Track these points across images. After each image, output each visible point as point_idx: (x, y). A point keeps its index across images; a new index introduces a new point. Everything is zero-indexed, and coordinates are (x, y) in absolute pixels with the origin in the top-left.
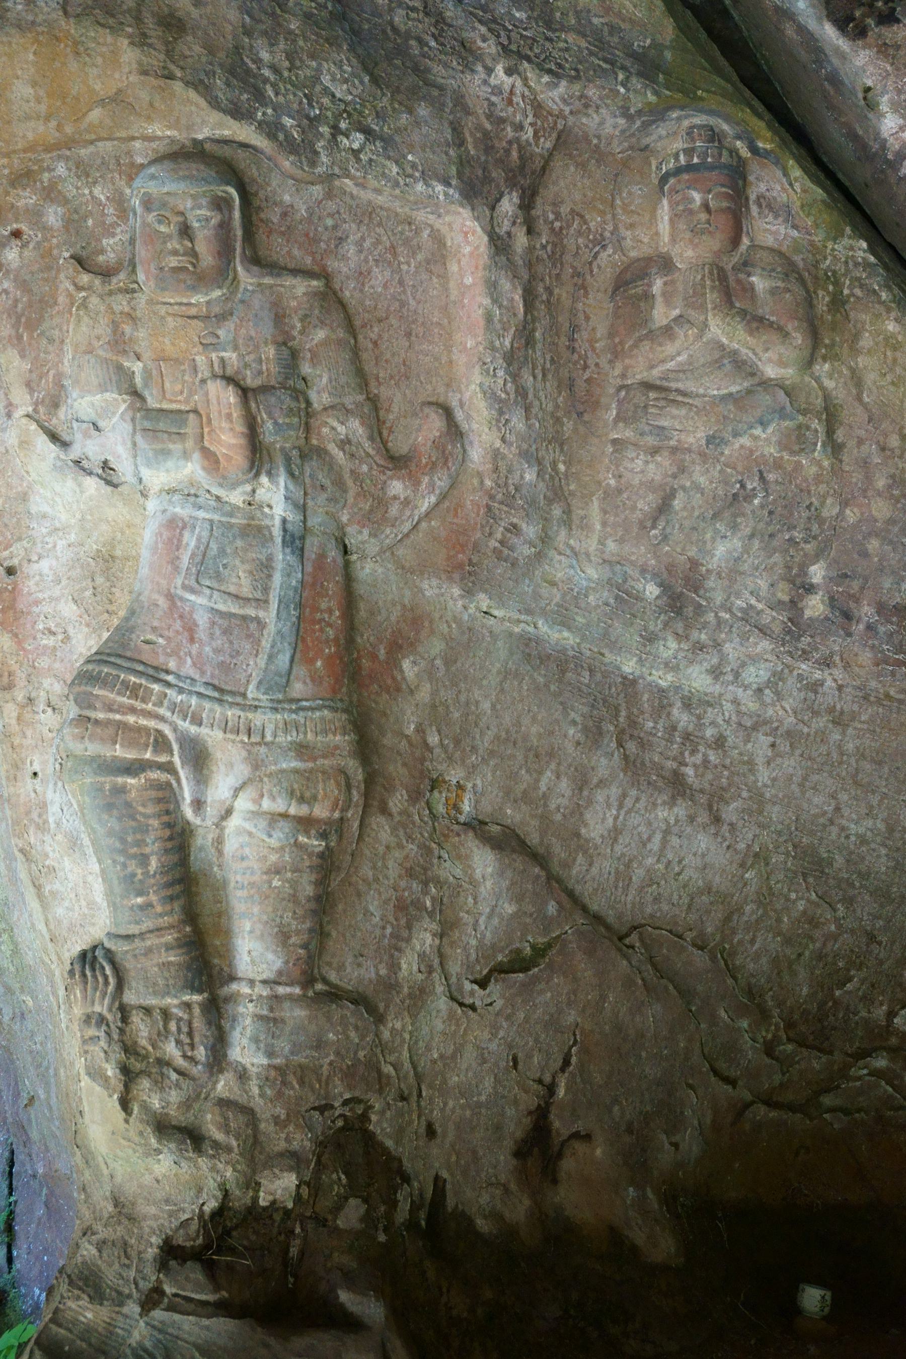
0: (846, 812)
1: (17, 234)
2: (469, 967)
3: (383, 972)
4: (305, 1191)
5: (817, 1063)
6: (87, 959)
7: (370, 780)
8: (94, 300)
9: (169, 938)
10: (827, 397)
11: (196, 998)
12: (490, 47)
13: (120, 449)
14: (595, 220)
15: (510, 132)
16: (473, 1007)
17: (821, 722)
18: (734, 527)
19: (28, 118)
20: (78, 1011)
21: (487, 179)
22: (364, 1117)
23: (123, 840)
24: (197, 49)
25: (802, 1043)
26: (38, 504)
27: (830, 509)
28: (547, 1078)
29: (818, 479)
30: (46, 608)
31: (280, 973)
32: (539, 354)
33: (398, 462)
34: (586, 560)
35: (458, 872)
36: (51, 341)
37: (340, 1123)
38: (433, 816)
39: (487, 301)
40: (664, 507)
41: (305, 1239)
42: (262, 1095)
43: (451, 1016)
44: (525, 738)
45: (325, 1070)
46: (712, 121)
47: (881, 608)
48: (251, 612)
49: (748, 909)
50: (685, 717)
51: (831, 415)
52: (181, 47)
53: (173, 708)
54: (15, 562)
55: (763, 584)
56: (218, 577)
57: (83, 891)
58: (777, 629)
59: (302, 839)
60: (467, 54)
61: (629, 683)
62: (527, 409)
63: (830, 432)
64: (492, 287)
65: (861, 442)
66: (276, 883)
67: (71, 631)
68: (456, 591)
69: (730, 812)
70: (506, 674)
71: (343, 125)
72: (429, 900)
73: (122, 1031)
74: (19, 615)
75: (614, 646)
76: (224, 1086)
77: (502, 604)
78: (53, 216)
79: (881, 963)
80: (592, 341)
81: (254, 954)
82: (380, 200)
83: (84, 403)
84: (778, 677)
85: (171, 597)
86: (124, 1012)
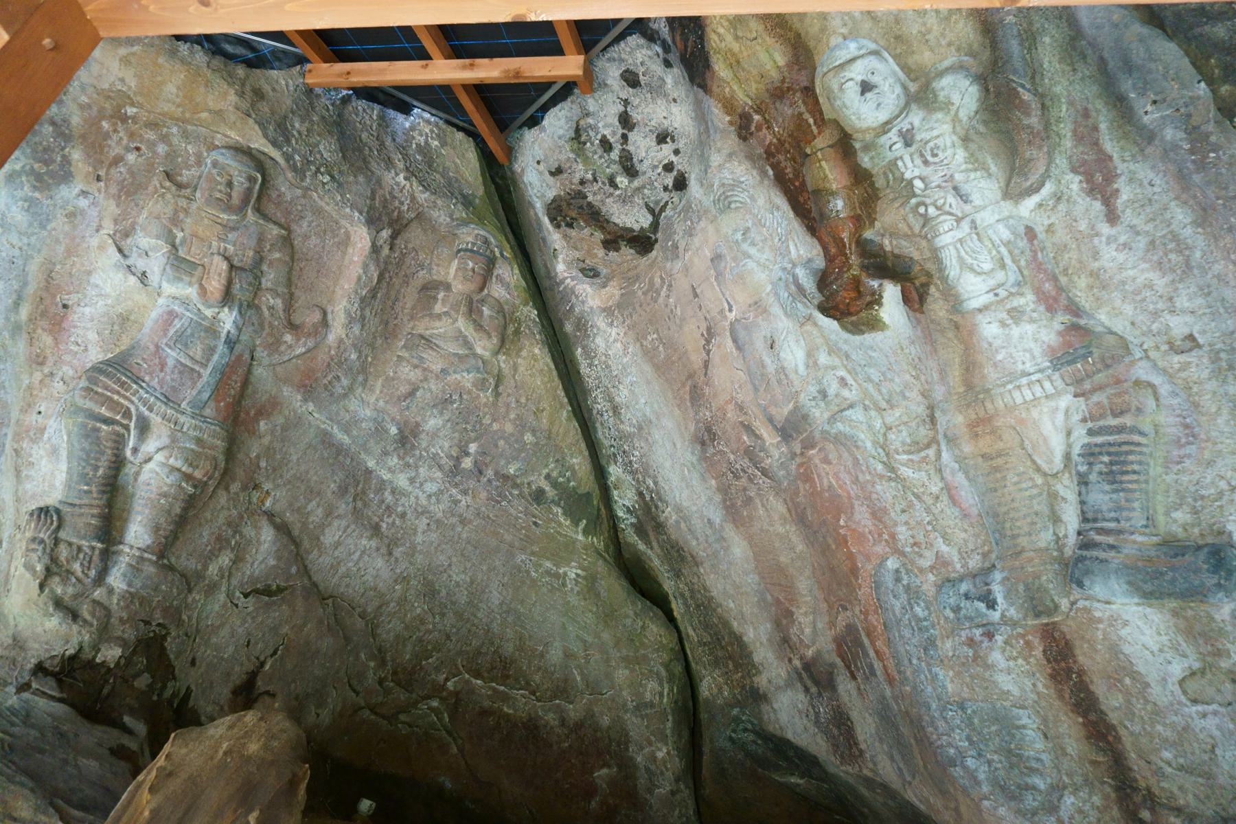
0: (453, 568)
1: (138, 149)
2: (242, 585)
3: (199, 567)
4: (123, 661)
5: (403, 696)
6: (44, 511)
7: (226, 472)
8: (169, 196)
9: (95, 511)
10: (500, 370)
11: (99, 545)
12: (401, 165)
13: (156, 269)
14: (422, 256)
15: (397, 203)
16: (237, 606)
17: (454, 520)
18: (441, 414)
19: (169, 101)
20: (28, 535)
21: (379, 219)
22: (164, 638)
23: (88, 455)
24: (266, 109)
25: (398, 684)
26: (96, 279)
27: (487, 420)
28: (262, 658)
29: (486, 405)
30: (79, 331)
31: (148, 547)
32: (377, 304)
33: (293, 327)
34: (366, 406)
35: (253, 534)
36: (137, 205)
37: (152, 635)
38: (250, 503)
39: (361, 271)
40: (412, 394)
41: (113, 687)
42: (118, 604)
43: (224, 605)
44: (308, 481)
45: (154, 604)
46: (487, 235)
47: (496, 473)
48: (197, 368)
49: (392, 605)
50: (390, 498)
51: (499, 379)
52: (259, 105)
53: (140, 399)
54: (70, 303)
55: (446, 445)
56: (186, 345)
57: (53, 474)
58: (447, 468)
59: (184, 484)
60: (389, 163)
61: (369, 472)
62: (363, 326)
63: (497, 386)
64: (365, 267)
65: (509, 395)
66: (162, 501)
67: (90, 347)
68: (299, 397)
69: (398, 552)
70: (310, 446)
71: (322, 170)
72: (232, 540)
73: (52, 550)
74: (62, 329)
75: (367, 451)
76: (98, 594)
77: (319, 412)
78: (161, 149)
79: (449, 651)
80: (403, 308)
81: (138, 533)
82: (327, 208)
83: (143, 240)
84: (441, 492)
85: (157, 347)
86: (57, 542)
